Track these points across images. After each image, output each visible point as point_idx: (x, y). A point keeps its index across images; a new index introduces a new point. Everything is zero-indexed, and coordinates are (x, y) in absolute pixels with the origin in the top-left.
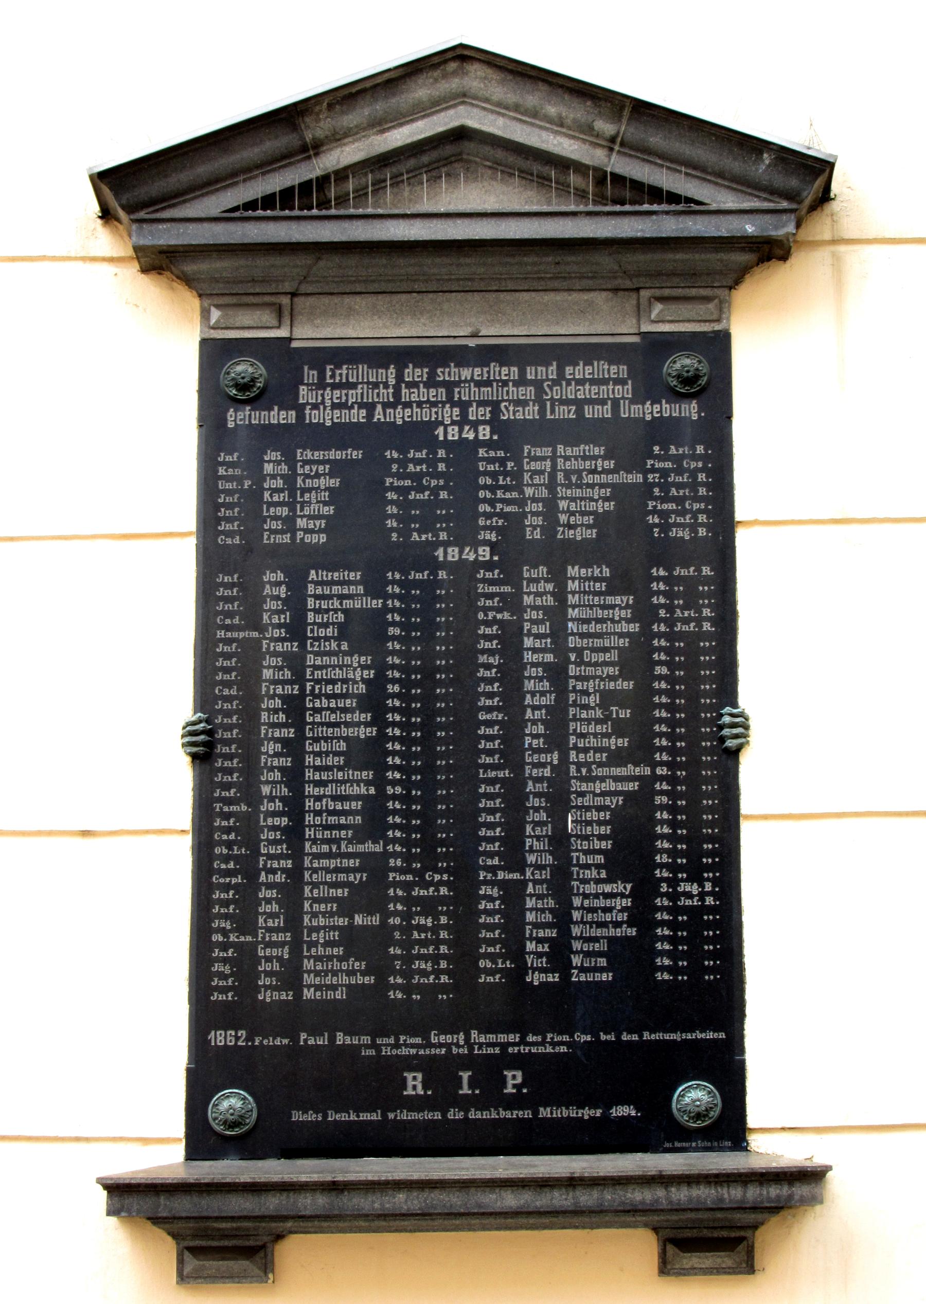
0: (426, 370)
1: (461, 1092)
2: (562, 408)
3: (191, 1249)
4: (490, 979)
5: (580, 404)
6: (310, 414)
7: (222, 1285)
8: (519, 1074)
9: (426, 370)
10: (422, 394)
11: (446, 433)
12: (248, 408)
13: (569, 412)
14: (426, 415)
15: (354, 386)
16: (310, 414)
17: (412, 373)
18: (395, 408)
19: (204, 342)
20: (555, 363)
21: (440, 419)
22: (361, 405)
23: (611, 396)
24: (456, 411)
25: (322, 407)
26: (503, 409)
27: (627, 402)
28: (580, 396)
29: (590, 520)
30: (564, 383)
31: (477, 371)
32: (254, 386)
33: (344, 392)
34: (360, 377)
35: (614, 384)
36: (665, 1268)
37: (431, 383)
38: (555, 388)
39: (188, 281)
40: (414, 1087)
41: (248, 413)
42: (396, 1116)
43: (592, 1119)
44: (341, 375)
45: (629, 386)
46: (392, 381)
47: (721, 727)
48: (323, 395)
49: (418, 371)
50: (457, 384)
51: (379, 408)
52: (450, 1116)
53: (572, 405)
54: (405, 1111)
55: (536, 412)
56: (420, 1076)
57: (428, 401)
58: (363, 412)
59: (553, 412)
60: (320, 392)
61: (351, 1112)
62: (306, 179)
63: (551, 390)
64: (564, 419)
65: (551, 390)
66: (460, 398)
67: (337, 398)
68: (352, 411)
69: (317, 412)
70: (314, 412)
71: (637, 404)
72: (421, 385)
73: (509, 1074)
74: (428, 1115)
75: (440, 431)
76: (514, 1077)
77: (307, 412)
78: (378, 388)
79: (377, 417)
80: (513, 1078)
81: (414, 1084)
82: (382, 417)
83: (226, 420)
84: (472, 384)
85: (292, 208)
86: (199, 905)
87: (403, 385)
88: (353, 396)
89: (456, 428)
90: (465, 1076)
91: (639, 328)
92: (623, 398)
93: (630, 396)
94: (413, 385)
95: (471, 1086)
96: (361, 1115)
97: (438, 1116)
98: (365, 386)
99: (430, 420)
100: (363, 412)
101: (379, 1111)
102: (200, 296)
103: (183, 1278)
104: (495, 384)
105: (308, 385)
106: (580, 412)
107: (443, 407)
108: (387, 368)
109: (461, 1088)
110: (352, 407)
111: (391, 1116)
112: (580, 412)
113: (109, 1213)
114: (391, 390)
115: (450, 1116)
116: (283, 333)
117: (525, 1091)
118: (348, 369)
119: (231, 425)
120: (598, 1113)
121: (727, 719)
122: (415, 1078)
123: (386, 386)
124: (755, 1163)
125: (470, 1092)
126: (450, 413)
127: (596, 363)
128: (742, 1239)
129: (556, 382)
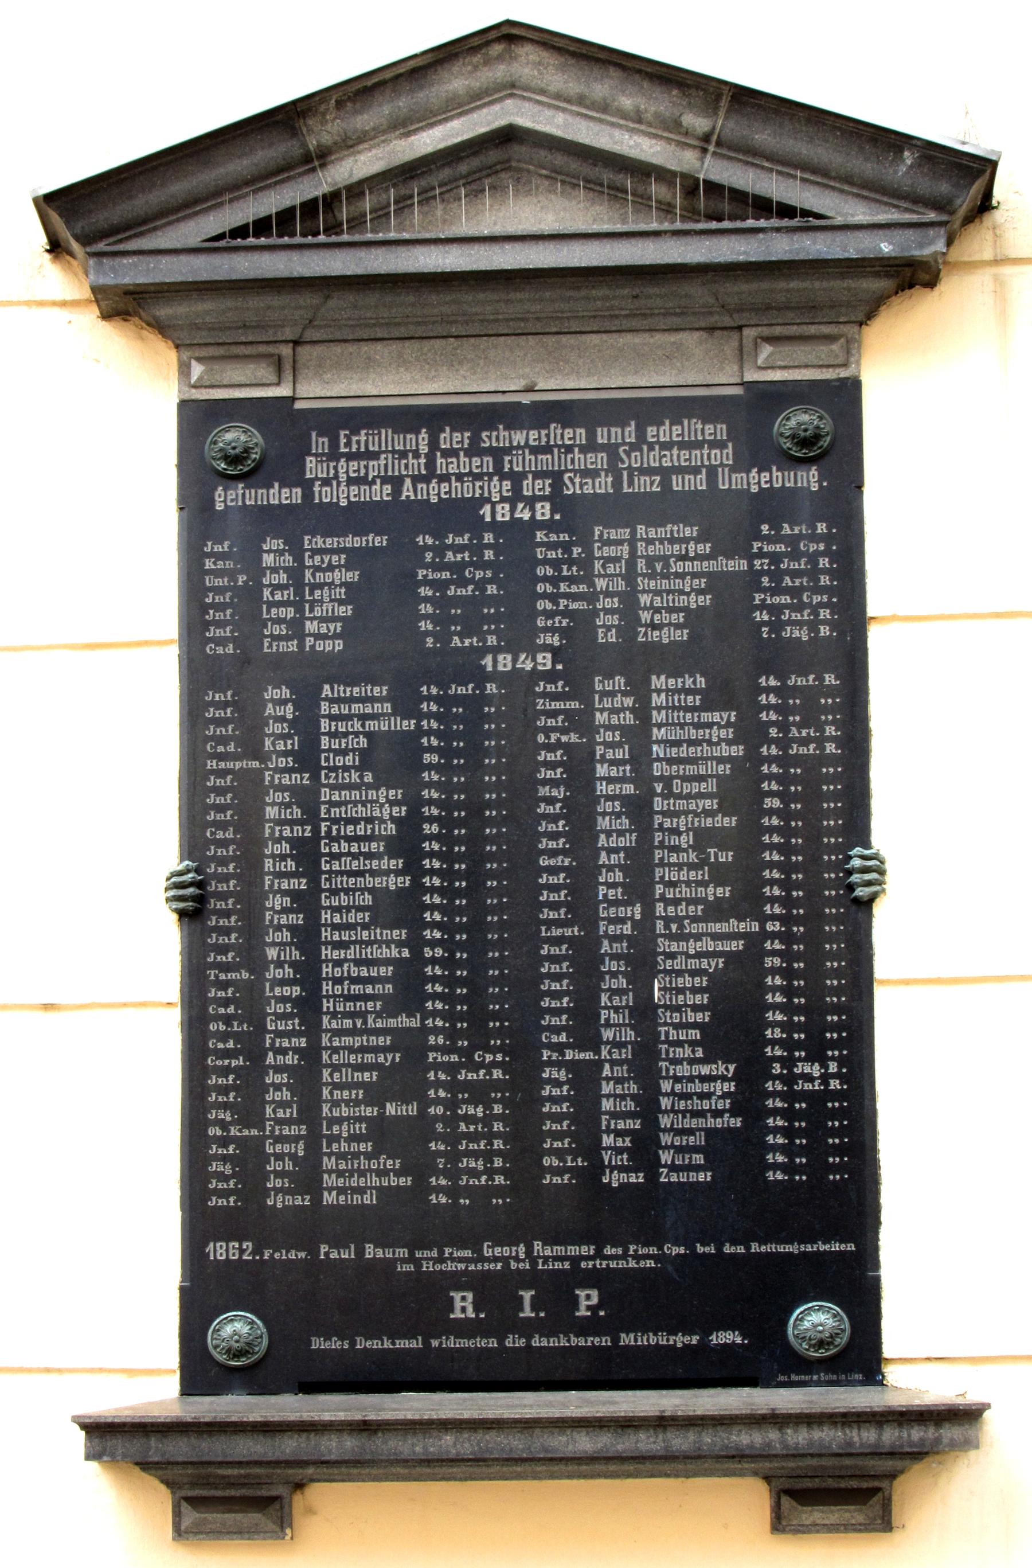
0: (467, 434)
2: (642, 478)
5: (665, 473)
8: (594, 1294)
9: (467, 434)
10: (463, 464)
11: (493, 513)
14: (467, 490)
15: (375, 456)
16: (320, 492)
17: (448, 438)
20: (633, 423)
23: (706, 463)
24: (507, 485)
25: (334, 483)
26: (567, 482)
27: (726, 470)
28: (666, 463)
32: (246, 458)
33: (363, 463)
35: (710, 448)
37: (474, 450)
38: (633, 455)
39: (162, 328)
40: (464, 1309)
41: (241, 492)
43: (687, 1347)
44: (358, 442)
45: (730, 450)
46: (424, 449)
50: (508, 450)
51: (408, 482)
56: (470, 1296)
58: (388, 489)
59: (631, 483)
60: (332, 464)
64: (645, 492)
66: (511, 468)
68: (374, 487)
69: (328, 489)
70: (324, 489)
74: (481, 1343)
75: (487, 510)
76: (588, 1297)
77: (316, 489)
79: (405, 494)
83: (213, 501)
87: (439, 454)
88: (374, 468)
90: (527, 1295)
94: (451, 453)
97: (493, 1343)
100: (388, 489)
101: (420, 1338)
102: (177, 347)
104: (556, 450)
105: (316, 455)
107: (490, 480)
108: (417, 433)
109: (522, 1310)
112: (666, 484)
117: (602, 1313)
118: (367, 434)
119: (219, 507)
120: (695, 1340)
122: (464, 1299)
126: (498, 488)
129: (635, 447)
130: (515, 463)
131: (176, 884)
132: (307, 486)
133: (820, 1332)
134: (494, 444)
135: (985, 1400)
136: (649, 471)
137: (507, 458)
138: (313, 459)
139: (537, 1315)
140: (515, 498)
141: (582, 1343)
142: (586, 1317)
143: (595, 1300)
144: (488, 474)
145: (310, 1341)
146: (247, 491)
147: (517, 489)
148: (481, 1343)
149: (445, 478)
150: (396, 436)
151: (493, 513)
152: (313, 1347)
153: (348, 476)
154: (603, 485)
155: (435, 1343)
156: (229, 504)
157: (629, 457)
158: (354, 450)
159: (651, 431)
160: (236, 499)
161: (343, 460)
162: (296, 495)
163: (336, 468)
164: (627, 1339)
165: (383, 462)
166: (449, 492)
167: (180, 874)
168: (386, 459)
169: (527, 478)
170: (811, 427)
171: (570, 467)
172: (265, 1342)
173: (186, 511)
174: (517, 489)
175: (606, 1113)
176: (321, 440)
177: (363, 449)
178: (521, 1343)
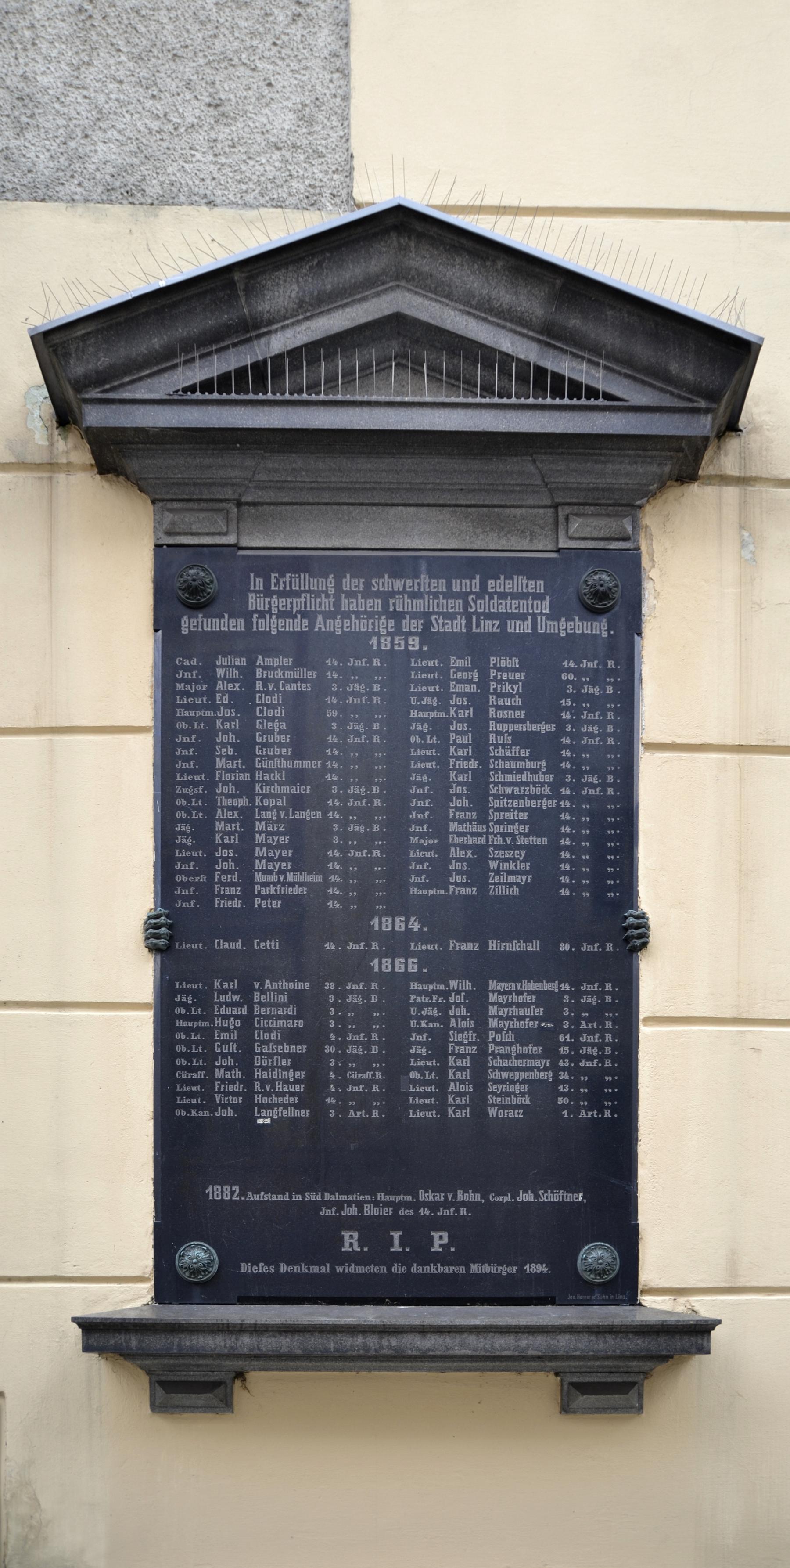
0: (362, 580)
1: (392, 1250)
2: (487, 622)
3: (162, 1383)
4: (356, 1089)
5: (504, 618)
6: (257, 622)
7: (178, 1416)
8: (445, 1235)
9: (362, 580)
10: (360, 604)
11: (379, 643)
12: (200, 615)
13: (493, 625)
14: (363, 626)
15: (297, 594)
16: (257, 622)
17: (349, 583)
18: (334, 618)
19: (158, 546)
20: (478, 577)
21: (376, 630)
22: (304, 614)
23: (531, 611)
24: (392, 623)
25: (268, 616)
26: (434, 622)
27: (544, 618)
28: (502, 610)
29: (524, 816)
30: (487, 597)
31: (409, 582)
32: (203, 591)
33: (289, 600)
34: (302, 585)
35: (533, 599)
36: (565, 1409)
37: (368, 593)
38: (479, 602)
39: (140, 485)
40: (351, 1245)
41: (200, 620)
42: (344, 1270)
43: (509, 1275)
44: (285, 583)
45: (547, 602)
46: (332, 591)
47: (626, 929)
48: (270, 603)
49: (355, 581)
50: (392, 594)
51: (320, 618)
52: (394, 1270)
53: (497, 619)
54: (353, 1265)
55: (463, 625)
56: (356, 1235)
57: (365, 612)
58: (305, 622)
59: (478, 626)
60: (267, 600)
61: (303, 1265)
62: (242, 364)
63: (475, 603)
64: (489, 633)
65: (475, 603)
66: (395, 609)
67: (283, 606)
68: (296, 620)
69: (263, 621)
70: (260, 621)
71: (553, 620)
72: (359, 595)
73: (436, 1235)
74: (373, 1269)
75: (374, 640)
76: (441, 1237)
77: (254, 620)
78: (320, 597)
79: (317, 626)
80: (440, 1239)
81: (350, 1240)
82: (322, 626)
83: (180, 626)
84: (406, 596)
85: (229, 392)
86: (162, 1078)
87: (343, 595)
88: (298, 604)
89: (389, 639)
90: (396, 1235)
91: (557, 543)
92: (541, 614)
93: (548, 611)
94: (351, 594)
95: (402, 1244)
96: (311, 1268)
97: (383, 1270)
98: (308, 595)
99: (367, 631)
100: (305, 622)
101: (328, 1265)
102: (153, 502)
103: (156, 1407)
104: (426, 596)
105: (256, 592)
106: (503, 626)
107: (379, 619)
108: (327, 578)
109: (392, 1245)
110: (296, 617)
111: (339, 1269)
112: (503, 626)
113: (87, 1348)
114: (332, 600)
115: (394, 1270)
116: (231, 539)
117: (453, 1249)
118: (291, 577)
119: (185, 631)
120: (514, 1269)
121: (631, 920)
122: (351, 1236)
123: (328, 596)
124: (637, 1316)
125: (401, 1250)
126: (385, 625)
127: (515, 577)
128: (633, 1384)
129: (480, 596)
130: (402, 604)
131: (152, 925)
132: (248, 616)
133: (601, 1264)
134: (381, 589)
135: (719, 1318)
136: (490, 616)
137: (391, 601)
138: (254, 595)
139: (404, 1249)
140: (398, 631)
141: (446, 1271)
142: (438, 1252)
143: (446, 1240)
144: (378, 613)
145: (240, 1267)
146: (205, 620)
147: (398, 626)
148: (373, 1269)
149: (346, 615)
150: (312, 580)
151: (379, 643)
152: (242, 1271)
153: (279, 610)
154: (458, 626)
155: (339, 1269)
156: (345, 629)
157: (476, 604)
158: (281, 589)
159: (491, 583)
160: (197, 626)
161: (275, 597)
162: (238, 625)
163: (270, 603)
164: (474, 1268)
165: (303, 600)
166: (236, 626)
167: (157, 917)
168: (305, 598)
169: (405, 618)
170: (606, 585)
171: (436, 610)
172: (216, 1266)
173: (160, 632)
174: (398, 626)
175: (218, 1080)
176: (257, 580)
177: (288, 588)
178: (404, 1269)
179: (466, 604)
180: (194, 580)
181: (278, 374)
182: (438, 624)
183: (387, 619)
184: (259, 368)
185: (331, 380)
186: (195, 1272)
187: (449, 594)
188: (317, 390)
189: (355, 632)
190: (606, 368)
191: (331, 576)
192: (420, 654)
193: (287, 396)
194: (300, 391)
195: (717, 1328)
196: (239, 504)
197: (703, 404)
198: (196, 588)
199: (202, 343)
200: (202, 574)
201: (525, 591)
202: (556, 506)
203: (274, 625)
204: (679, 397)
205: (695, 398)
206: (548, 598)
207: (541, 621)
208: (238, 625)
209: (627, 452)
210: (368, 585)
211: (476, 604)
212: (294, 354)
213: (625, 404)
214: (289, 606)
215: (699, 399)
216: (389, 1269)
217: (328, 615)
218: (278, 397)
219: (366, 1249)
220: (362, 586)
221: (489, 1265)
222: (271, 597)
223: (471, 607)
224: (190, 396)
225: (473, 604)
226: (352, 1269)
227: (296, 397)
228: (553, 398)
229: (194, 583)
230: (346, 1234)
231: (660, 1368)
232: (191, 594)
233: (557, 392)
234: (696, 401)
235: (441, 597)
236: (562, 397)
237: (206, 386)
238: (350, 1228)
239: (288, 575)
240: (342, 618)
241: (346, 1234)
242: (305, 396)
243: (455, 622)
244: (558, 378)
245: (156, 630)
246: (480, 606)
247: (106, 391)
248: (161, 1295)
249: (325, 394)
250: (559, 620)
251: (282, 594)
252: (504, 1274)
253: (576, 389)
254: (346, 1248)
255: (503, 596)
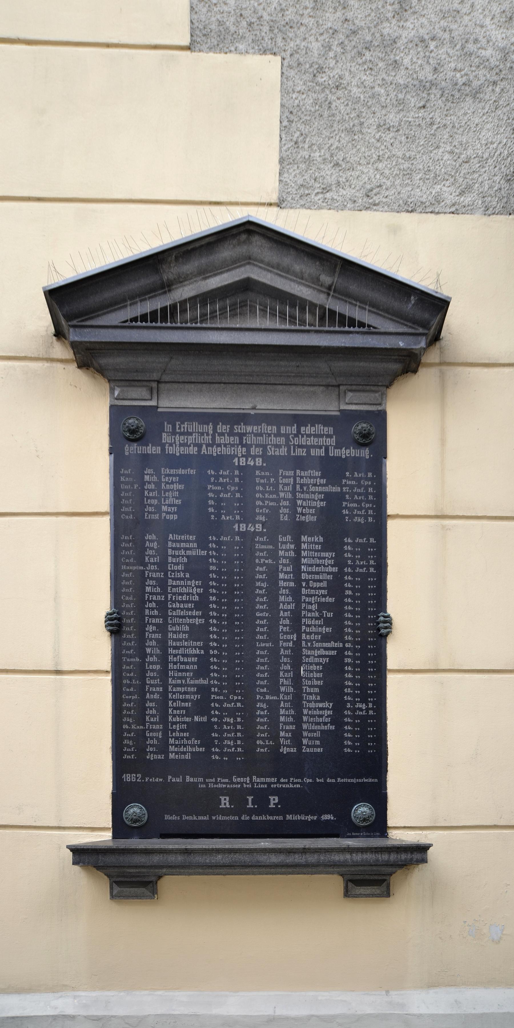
0: (228, 426)
5: (308, 448)
8: (276, 798)
9: (228, 426)
10: (227, 439)
12: (135, 444)
14: (228, 451)
15: (191, 434)
17: (221, 428)
18: (212, 447)
19: (112, 407)
20: (295, 425)
24: (244, 449)
25: (174, 445)
26: (269, 449)
30: (300, 436)
32: (137, 431)
33: (185, 437)
37: (231, 434)
38: (295, 439)
39: (101, 371)
40: (225, 804)
41: (135, 447)
44: (184, 428)
46: (211, 432)
48: (175, 439)
49: (224, 427)
50: (244, 434)
51: (204, 446)
56: (228, 798)
57: (230, 444)
59: (294, 451)
60: (173, 437)
66: (246, 442)
72: (226, 435)
73: (271, 798)
74: (232, 818)
76: (274, 799)
77: (167, 447)
80: (274, 800)
81: (225, 802)
88: (191, 440)
90: (250, 798)
102: (109, 381)
104: (264, 436)
105: (167, 432)
106: (308, 452)
107: (238, 447)
109: (248, 804)
110: (190, 446)
114: (210, 437)
116: (153, 403)
118: (187, 424)
119: (127, 454)
122: (225, 799)
123: (208, 435)
124: (389, 843)
129: (296, 436)
132: (163, 446)
135: (428, 842)
141: (272, 819)
143: (277, 801)
149: (219, 445)
154: (283, 451)
155: (214, 818)
157: (294, 440)
159: (303, 429)
161: (177, 435)
162: (158, 450)
163: (175, 439)
165: (194, 437)
174: (248, 451)
176: (168, 426)
179: (288, 440)
180: (132, 426)
181: (184, 311)
182: (271, 451)
183: (242, 447)
184: (173, 307)
185: (204, 315)
186: (135, 821)
187: (278, 434)
188: (196, 321)
189: (187, 455)
190: (369, 311)
191: (211, 424)
192: (261, 468)
193: (179, 325)
194: (186, 323)
195: (431, 848)
196: (159, 382)
197: (421, 330)
198: (134, 430)
199: (140, 295)
200: (136, 422)
201: (322, 433)
202: (339, 386)
203: (177, 451)
204: (410, 327)
205: (417, 327)
206: (334, 437)
207: (331, 450)
208: (158, 450)
209: (377, 356)
210: (232, 429)
211: (294, 440)
212: (193, 299)
213: (376, 330)
214: (186, 441)
215: (419, 328)
216: (240, 818)
217: (208, 445)
218: (174, 325)
219: (256, 806)
220: (228, 430)
221: (300, 815)
222: (176, 435)
223: (291, 442)
224: (124, 324)
225: (292, 440)
226: (220, 818)
227: (184, 325)
228: (339, 326)
229: (132, 428)
230: (222, 798)
231: (399, 872)
232: (131, 433)
233: (342, 324)
234: (417, 329)
235: (273, 436)
236: (147, 322)
237: (144, 318)
238: (223, 795)
239: (186, 423)
240: (217, 447)
241: (222, 798)
242: (189, 325)
243: (281, 450)
244: (342, 316)
245: (111, 454)
246: (296, 441)
247: (83, 321)
248: (115, 836)
249: (170, 322)
250: (341, 449)
251: (181, 434)
252: (309, 820)
253: (352, 322)
254: (222, 806)
255: (309, 436)
